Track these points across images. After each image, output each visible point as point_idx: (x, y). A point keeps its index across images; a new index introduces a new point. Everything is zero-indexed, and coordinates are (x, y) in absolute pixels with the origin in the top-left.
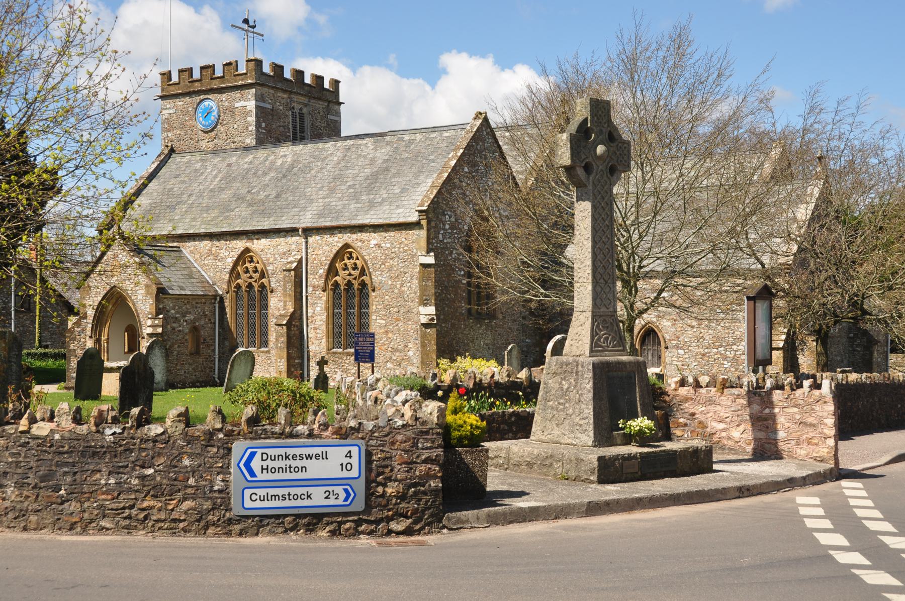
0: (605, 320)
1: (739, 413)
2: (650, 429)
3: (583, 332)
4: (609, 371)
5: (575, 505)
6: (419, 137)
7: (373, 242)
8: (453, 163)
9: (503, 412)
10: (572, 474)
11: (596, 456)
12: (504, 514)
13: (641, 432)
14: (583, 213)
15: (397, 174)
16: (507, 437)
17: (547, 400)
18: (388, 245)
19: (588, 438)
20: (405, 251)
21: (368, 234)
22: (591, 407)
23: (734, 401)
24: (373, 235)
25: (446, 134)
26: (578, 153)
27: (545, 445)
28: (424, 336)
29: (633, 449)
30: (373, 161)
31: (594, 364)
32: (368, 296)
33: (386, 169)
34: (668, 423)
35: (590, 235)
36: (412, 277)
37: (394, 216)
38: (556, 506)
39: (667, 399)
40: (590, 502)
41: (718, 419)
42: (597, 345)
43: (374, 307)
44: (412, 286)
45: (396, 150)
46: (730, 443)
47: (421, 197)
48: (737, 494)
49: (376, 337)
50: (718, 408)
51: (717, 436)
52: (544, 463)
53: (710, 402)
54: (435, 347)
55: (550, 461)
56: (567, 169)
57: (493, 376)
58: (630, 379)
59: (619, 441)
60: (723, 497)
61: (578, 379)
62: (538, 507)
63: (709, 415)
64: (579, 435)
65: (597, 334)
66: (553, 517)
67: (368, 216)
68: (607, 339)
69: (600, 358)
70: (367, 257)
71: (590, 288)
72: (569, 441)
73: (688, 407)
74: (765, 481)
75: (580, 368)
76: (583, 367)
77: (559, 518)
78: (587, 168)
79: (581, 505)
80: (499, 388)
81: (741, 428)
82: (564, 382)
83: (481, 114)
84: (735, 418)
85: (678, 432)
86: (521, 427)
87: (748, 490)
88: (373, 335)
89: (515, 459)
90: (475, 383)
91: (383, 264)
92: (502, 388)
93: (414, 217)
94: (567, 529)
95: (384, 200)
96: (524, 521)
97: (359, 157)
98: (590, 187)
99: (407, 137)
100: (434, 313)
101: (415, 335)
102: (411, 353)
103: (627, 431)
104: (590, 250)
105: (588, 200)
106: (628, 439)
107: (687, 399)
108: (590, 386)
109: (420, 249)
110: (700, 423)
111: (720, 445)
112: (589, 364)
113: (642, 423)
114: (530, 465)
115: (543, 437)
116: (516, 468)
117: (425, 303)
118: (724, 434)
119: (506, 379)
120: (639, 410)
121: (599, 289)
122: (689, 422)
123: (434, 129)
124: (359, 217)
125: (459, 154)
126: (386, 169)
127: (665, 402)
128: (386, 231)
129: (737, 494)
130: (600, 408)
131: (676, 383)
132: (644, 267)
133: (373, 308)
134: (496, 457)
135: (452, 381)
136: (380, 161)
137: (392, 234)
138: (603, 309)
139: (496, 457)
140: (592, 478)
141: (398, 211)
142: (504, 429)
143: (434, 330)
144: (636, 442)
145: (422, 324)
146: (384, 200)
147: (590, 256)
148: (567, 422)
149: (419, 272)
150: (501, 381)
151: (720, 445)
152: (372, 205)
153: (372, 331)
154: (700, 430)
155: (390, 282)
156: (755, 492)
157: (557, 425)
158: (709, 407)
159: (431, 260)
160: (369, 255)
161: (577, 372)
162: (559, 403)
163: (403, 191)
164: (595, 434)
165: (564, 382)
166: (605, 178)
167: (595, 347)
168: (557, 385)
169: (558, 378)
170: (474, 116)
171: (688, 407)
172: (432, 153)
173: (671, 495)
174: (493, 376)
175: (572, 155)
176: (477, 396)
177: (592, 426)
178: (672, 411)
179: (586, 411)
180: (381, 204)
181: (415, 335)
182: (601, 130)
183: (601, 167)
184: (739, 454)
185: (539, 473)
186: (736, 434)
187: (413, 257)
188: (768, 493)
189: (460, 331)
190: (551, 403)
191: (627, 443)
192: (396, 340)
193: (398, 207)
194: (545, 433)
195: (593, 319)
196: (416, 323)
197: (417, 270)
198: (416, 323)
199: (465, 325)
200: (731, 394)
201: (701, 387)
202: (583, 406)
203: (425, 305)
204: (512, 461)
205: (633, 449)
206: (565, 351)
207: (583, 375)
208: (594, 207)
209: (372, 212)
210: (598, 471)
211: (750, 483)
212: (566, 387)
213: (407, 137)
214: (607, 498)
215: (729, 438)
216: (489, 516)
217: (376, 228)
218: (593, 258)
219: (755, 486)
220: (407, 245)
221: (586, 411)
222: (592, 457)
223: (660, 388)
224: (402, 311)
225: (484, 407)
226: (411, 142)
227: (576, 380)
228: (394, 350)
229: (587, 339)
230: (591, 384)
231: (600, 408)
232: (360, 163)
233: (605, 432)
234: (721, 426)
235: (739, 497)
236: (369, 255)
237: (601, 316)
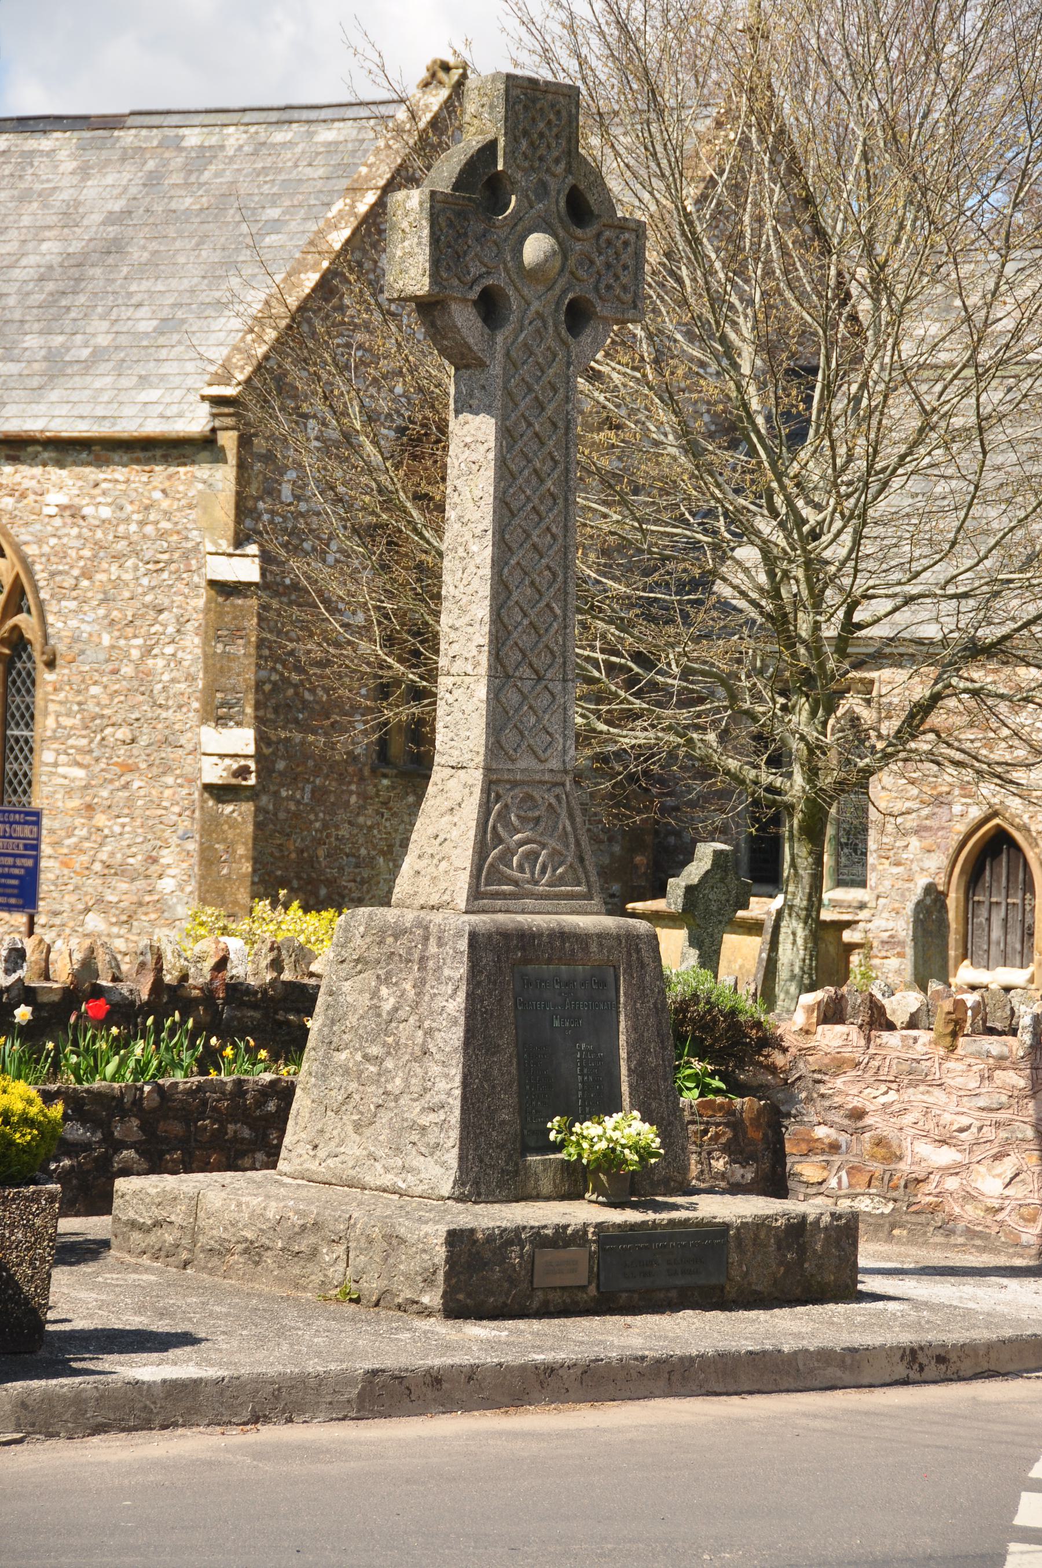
0: (528, 797)
1: (1002, 1116)
2: (644, 1153)
3: (455, 833)
4: (526, 961)
5: (321, 1380)
6: (234, 137)
7: (56, 498)
8: (338, 238)
9: (239, 1083)
10: (372, 1286)
11: (443, 1229)
12: (78, 1401)
13: (611, 1159)
14: (473, 443)
15: (152, 267)
16: (247, 1161)
17: (332, 1046)
18: (106, 512)
19: (440, 1171)
20: (162, 535)
21: (38, 471)
22: (456, 1073)
23: (986, 1077)
24: (55, 473)
25: (326, 135)
26: (458, 256)
27: (314, 1190)
28: (211, 827)
29: (585, 1213)
30: (70, 217)
31: (473, 937)
32: (30, 681)
33: (114, 248)
34: (782, 1142)
35: (488, 523)
36: (181, 623)
37: (128, 411)
38: (259, 1381)
39: (779, 1060)
40: (375, 1373)
41: (935, 1133)
42: (496, 876)
43: (51, 722)
44: (183, 655)
45: (153, 181)
46: (971, 1212)
47: (225, 351)
48: (901, 1371)
49: (45, 822)
50: (938, 1096)
51: (930, 1187)
52: (295, 1246)
53: (913, 1076)
54: (247, 867)
55: (312, 1240)
56: (428, 307)
57: (222, 964)
58: (601, 984)
59: (546, 1186)
60: (847, 1378)
61: (423, 981)
62: (197, 1382)
63: (908, 1119)
64: (418, 1162)
65: (498, 840)
66: (246, 1415)
67: (41, 409)
68: (532, 857)
69: (501, 917)
70: (31, 550)
71: (481, 691)
72: (387, 1180)
73: (847, 1091)
74: (1008, 1333)
75: (433, 949)
76: (440, 944)
77: (266, 1420)
78: (490, 307)
79: (344, 1379)
80: (242, 1005)
81: (1007, 1166)
82: (384, 991)
83: (446, 67)
84: (988, 1133)
85: (808, 1170)
86: (246, 1133)
87: (941, 1359)
88: (35, 818)
89: (213, 1233)
90: (158, 985)
91: (87, 574)
92: (255, 1006)
93: (195, 421)
94: (260, 1454)
95: (98, 355)
96: (146, 1425)
97: (24, 197)
98: (496, 369)
99: (193, 138)
100: (251, 750)
101: (185, 824)
102: (167, 885)
103: (569, 1154)
104: (487, 571)
105: (488, 410)
106: (574, 1182)
107: (839, 1065)
108: (456, 1005)
109: (210, 529)
110: (879, 1142)
111: (939, 1218)
112: (458, 935)
113: (626, 1130)
114: (254, 1252)
115: (313, 1166)
116: (215, 1261)
117: (219, 715)
118: (952, 1183)
119: (269, 977)
120: (625, 1088)
121: (512, 697)
122: (843, 1138)
123: (285, 114)
124: (10, 410)
125: (362, 208)
126: (114, 248)
127: (773, 1069)
128: (100, 462)
129: (901, 1371)
130: (487, 1075)
131: (810, 1010)
132: (860, 626)
133: (46, 724)
134: (157, 1224)
135: (75, 975)
136: (97, 218)
137: (120, 473)
138: (526, 762)
139: (157, 1224)
140: (426, 1300)
141: (145, 396)
142: (236, 1139)
143: (247, 808)
144: (599, 1189)
145: (208, 788)
146: (98, 355)
147: (486, 590)
148: (384, 1117)
149: (207, 610)
150: (252, 981)
151: (939, 1218)
152: (56, 368)
153: (36, 803)
154: (877, 1167)
155: (106, 640)
156: (967, 1367)
157: (358, 1127)
158: (910, 1093)
159: (246, 569)
160: (40, 542)
161: (423, 960)
162: (366, 1057)
163: (167, 325)
164: (462, 1158)
165: (384, 991)
166: (551, 341)
167: (487, 880)
168: (365, 1000)
169: (369, 977)
170: (423, 74)
171: (847, 1091)
172: (274, 200)
173: (658, 1361)
174: (222, 964)
175: (436, 262)
176: (158, 1027)
177: (455, 1134)
178: (792, 1100)
179: (442, 1085)
180: (87, 366)
181: (185, 824)
182: (543, 185)
183: (536, 306)
184: (996, 1251)
185: (279, 1279)
186: (990, 1183)
187: (186, 556)
188: (1017, 1374)
189: (342, 815)
190: (343, 1056)
191: (575, 1195)
192: (122, 838)
193: (144, 381)
194: (322, 1153)
195: (487, 790)
196: (191, 781)
197: (201, 603)
198: (191, 781)
199: (364, 796)
200: (977, 1055)
201: (891, 1027)
202: (435, 1069)
203: (221, 721)
204: (202, 1240)
205: (585, 1213)
206: (402, 886)
207: (438, 969)
208: (506, 435)
209: (54, 396)
210: (448, 1276)
211: (955, 1336)
212: (387, 1006)
213: (193, 138)
214: (436, 1361)
215: (969, 1197)
216: (24, 1405)
217: (66, 450)
218: (495, 596)
219: (967, 1350)
220: (167, 514)
221: (442, 1085)
222: (430, 1237)
223: (758, 1025)
224: (143, 741)
225: (177, 1065)
226: (205, 155)
227: (420, 985)
228: (112, 870)
229: (463, 856)
230: (461, 996)
231: (487, 1075)
232: (26, 220)
233: (496, 1159)
234: (946, 1156)
235: (905, 1382)
236: (40, 542)
237: (515, 784)
